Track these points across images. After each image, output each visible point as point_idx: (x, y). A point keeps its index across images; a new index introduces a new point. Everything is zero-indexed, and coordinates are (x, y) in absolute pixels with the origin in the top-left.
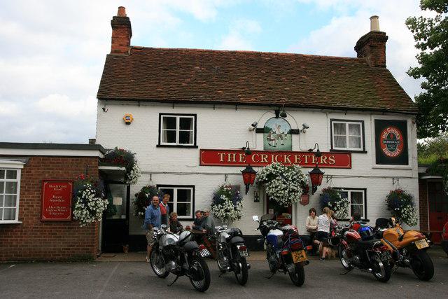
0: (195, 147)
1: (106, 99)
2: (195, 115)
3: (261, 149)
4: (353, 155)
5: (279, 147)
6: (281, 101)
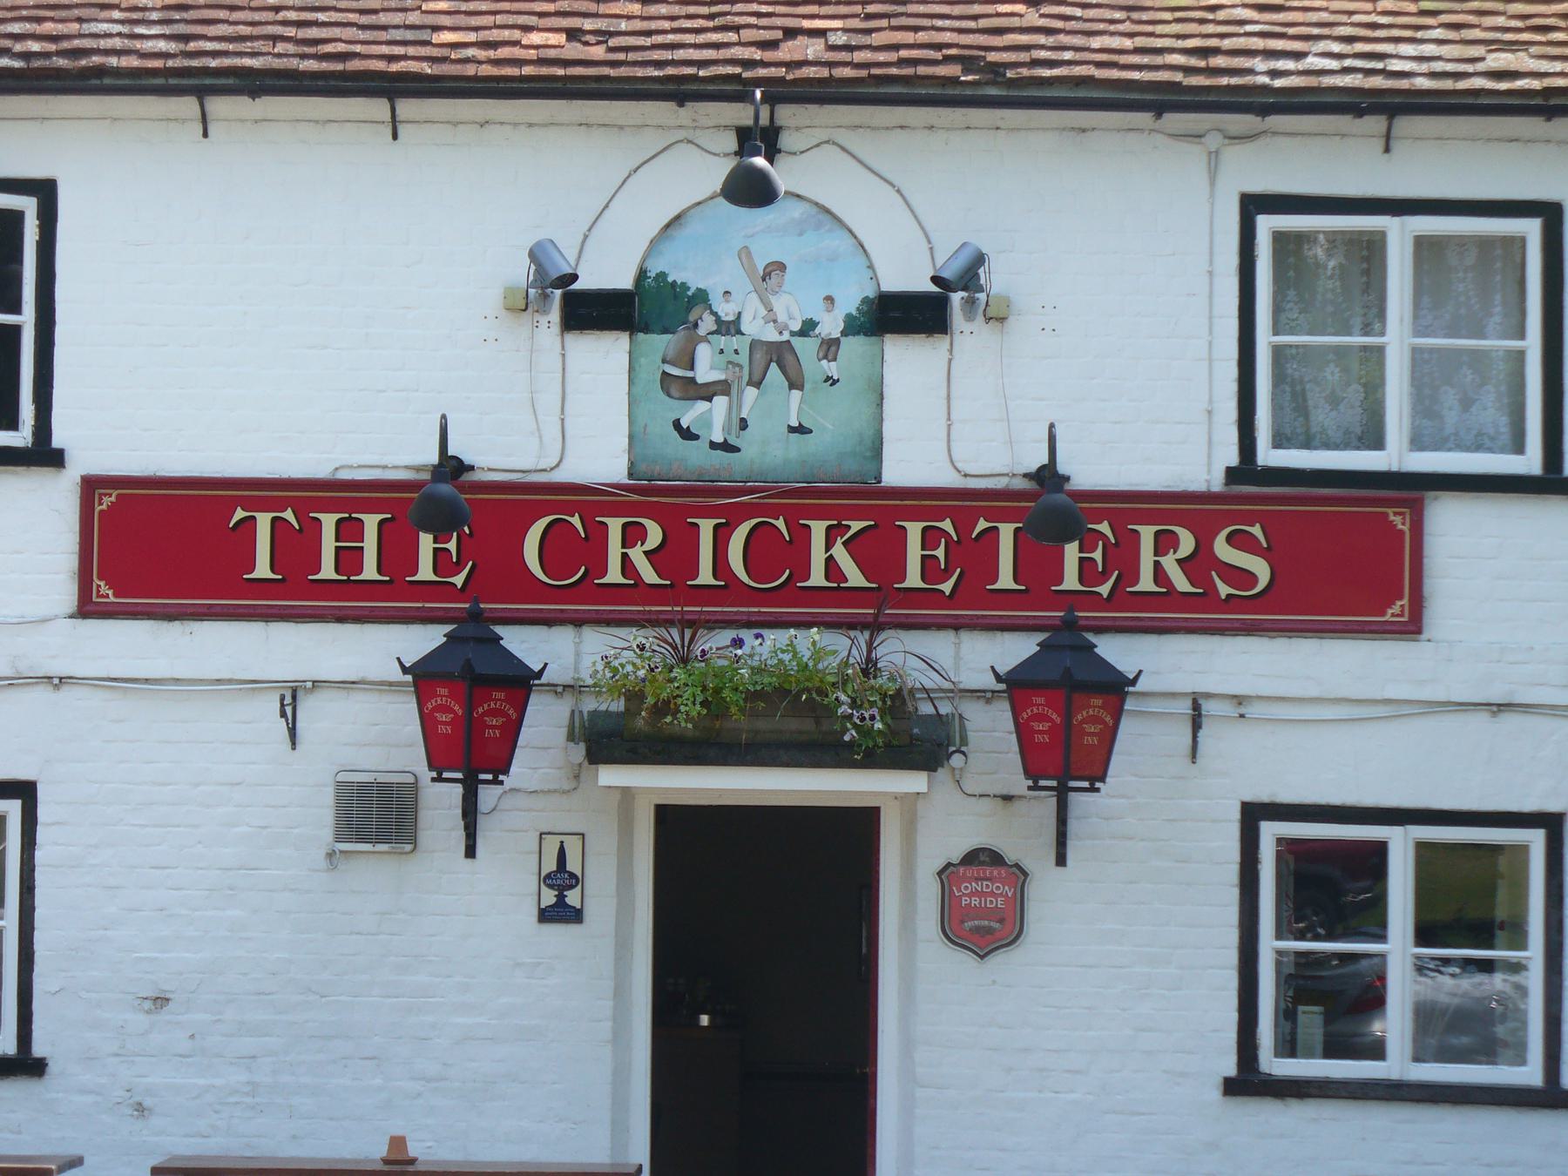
0: (43, 455)
2: (45, 191)
3: (600, 459)
6: (789, 50)
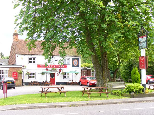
1: (18, 54)
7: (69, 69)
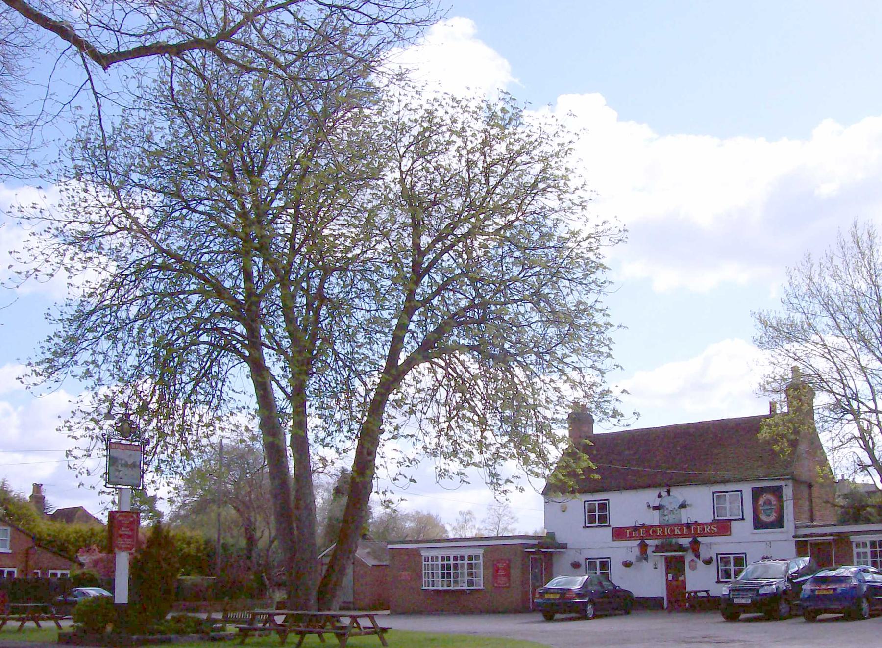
3: (657, 523)
4: (733, 523)
5: (671, 521)
7: (743, 537)
